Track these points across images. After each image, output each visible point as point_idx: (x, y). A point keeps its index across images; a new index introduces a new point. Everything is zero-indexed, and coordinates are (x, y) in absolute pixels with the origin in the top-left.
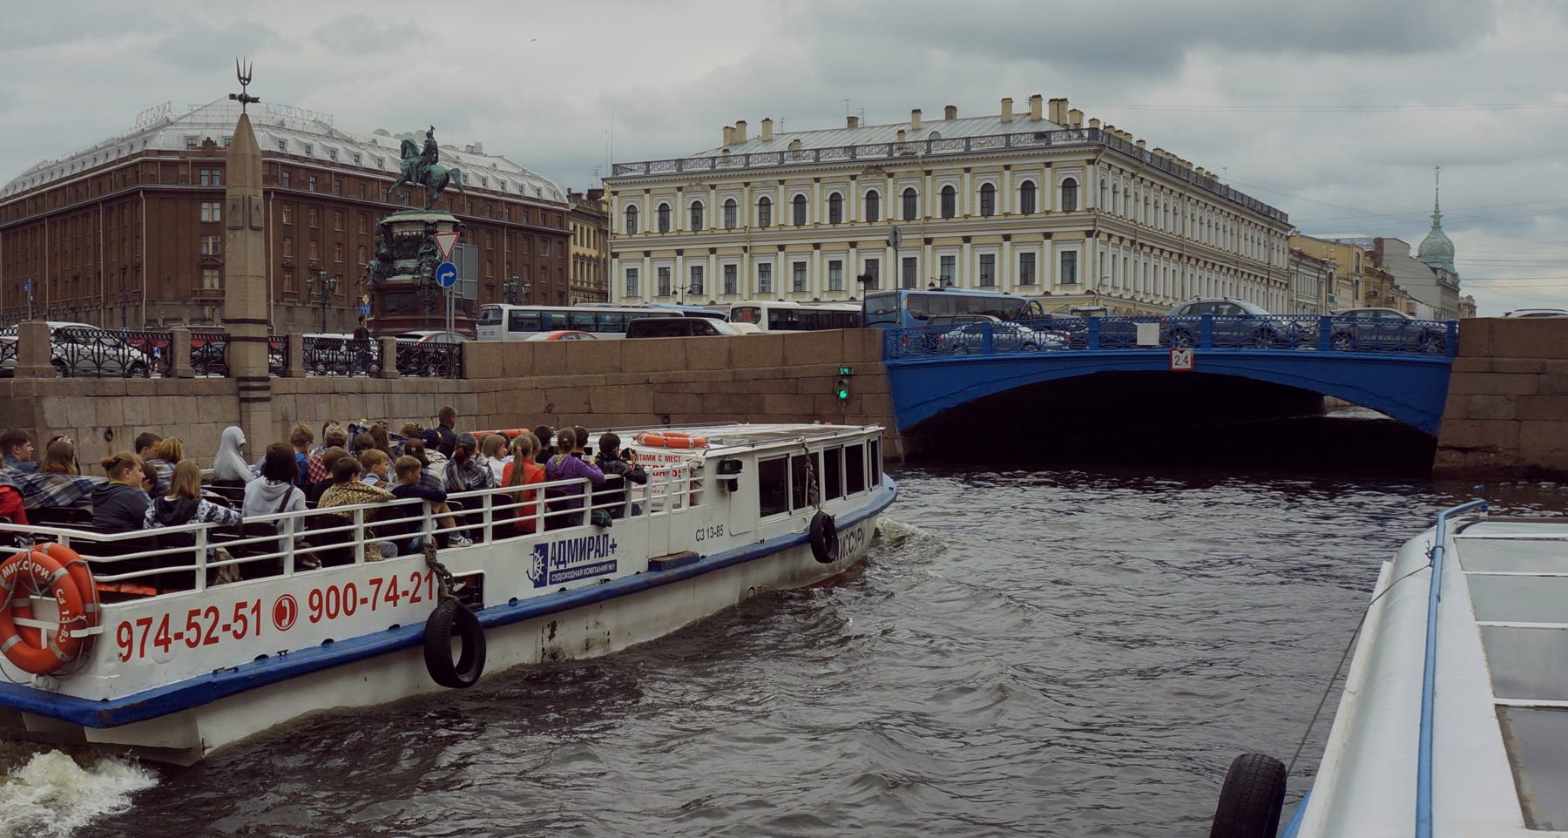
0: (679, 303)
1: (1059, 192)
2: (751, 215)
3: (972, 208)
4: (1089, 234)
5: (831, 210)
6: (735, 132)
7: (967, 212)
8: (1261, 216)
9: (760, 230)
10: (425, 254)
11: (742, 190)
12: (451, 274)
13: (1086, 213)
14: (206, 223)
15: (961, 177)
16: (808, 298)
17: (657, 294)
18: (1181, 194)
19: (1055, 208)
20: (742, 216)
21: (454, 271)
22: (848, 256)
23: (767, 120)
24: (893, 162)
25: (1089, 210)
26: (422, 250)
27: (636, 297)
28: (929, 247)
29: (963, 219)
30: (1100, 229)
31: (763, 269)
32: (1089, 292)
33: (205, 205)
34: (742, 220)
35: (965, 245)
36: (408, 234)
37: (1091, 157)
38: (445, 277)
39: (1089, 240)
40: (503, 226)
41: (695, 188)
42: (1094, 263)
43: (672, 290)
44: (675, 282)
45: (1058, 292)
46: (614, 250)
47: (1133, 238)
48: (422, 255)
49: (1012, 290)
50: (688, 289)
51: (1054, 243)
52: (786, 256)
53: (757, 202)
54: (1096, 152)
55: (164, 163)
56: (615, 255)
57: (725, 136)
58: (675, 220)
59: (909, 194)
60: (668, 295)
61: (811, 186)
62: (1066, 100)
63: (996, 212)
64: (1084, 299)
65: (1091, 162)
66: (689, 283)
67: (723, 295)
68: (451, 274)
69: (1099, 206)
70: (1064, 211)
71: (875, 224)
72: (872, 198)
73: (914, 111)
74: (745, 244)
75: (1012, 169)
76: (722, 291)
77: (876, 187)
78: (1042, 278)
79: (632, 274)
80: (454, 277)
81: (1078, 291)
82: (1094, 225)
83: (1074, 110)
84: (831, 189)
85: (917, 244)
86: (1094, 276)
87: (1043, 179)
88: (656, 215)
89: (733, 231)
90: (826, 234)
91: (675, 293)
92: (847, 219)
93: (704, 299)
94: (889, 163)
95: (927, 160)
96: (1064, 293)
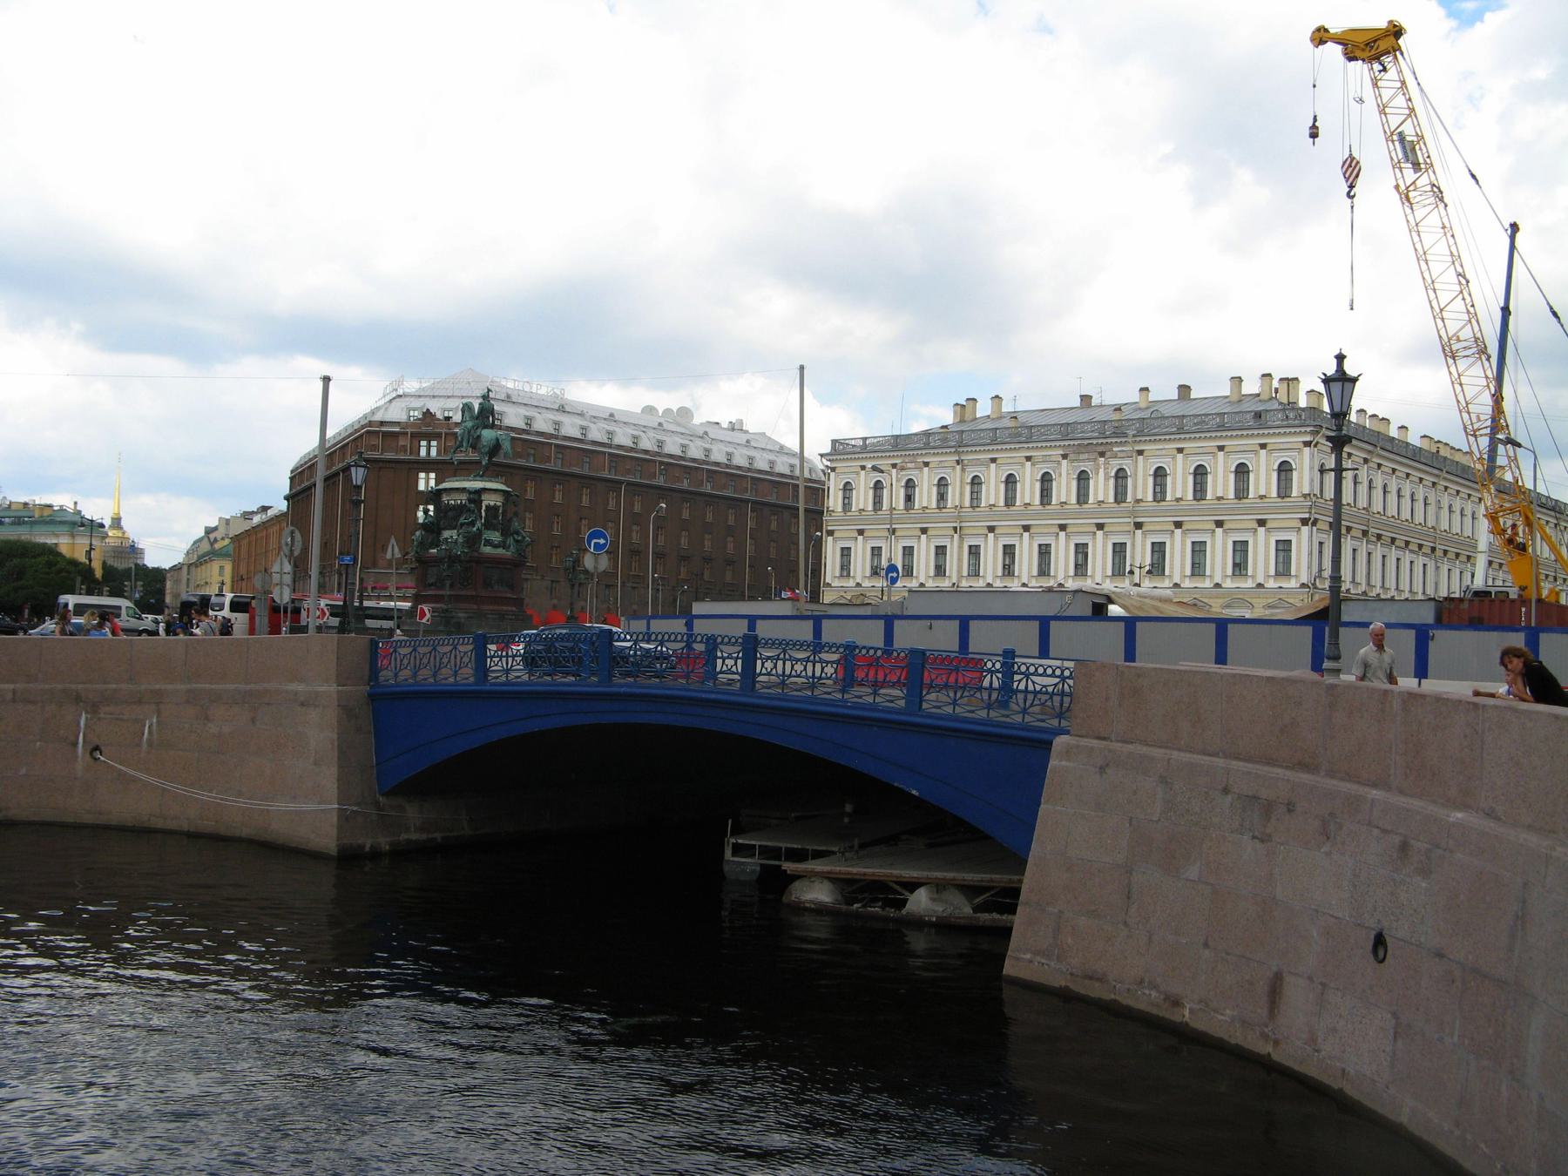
0: (1136, 585)
1: (1232, 476)
2: (962, 494)
3: (1144, 491)
4: (1304, 522)
5: (1042, 491)
6: (964, 409)
7: (1262, 492)
8: (1544, 510)
9: (971, 510)
10: (465, 523)
11: (954, 468)
12: (602, 541)
13: (1302, 499)
14: (422, 492)
15: (1174, 458)
16: (1167, 583)
17: (1000, 574)
18: (1434, 484)
19: (1034, 501)
20: (953, 496)
21: (606, 539)
22: (919, 541)
23: (997, 397)
24: (1104, 441)
25: (1305, 496)
26: (462, 520)
27: (1085, 575)
28: (1139, 532)
29: (1175, 503)
30: (1317, 516)
31: (973, 550)
32: (1303, 586)
33: (422, 475)
34: (953, 500)
35: (1176, 531)
36: (453, 502)
37: (1308, 438)
38: (595, 543)
39: (1305, 530)
40: (747, 501)
41: (909, 465)
42: (1310, 554)
43: (1128, 569)
44: (1133, 557)
45: (1271, 584)
46: (829, 528)
47: (1365, 528)
48: (462, 525)
49: (1104, 581)
50: (1147, 568)
51: (1268, 530)
52: (1031, 537)
53: (969, 481)
54: (1312, 433)
55: (386, 434)
56: (830, 533)
57: (955, 413)
58: (921, 497)
59: (1200, 471)
60: (1125, 575)
61: (1023, 465)
62: (1297, 379)
63: (1169, 498)
64: (1297, 593)
65: (1307, 444)
66: (1148, 561)
67: (839, 577)
68: (602, 541)
69: (1317, 491)
70: (971, 507)
71: (1085, 506)
72: (1083, 478)
73: (1142, 390)
74: (955, 525)
75: (1226, 450)
76: (932, 573)
77: (980, 472)
78: (1255, 569)
79: (846, 552)
80: (605, 545)
81: (1293, 583)
82: (1310, 513)
83: (1313, 391)
84: (1041, 468)
85: (1127, 528)
86: (1310, 567)
87: (1216, 463)
88: (871, 492)
89: (944, 510)
90: (1037, 516)
91: (1131, 572)
92: (1057, 500)
93: (1016, 580)
94: (1100, 441)
95: (1138, 439)
96: (1277, 585)
